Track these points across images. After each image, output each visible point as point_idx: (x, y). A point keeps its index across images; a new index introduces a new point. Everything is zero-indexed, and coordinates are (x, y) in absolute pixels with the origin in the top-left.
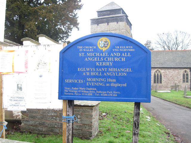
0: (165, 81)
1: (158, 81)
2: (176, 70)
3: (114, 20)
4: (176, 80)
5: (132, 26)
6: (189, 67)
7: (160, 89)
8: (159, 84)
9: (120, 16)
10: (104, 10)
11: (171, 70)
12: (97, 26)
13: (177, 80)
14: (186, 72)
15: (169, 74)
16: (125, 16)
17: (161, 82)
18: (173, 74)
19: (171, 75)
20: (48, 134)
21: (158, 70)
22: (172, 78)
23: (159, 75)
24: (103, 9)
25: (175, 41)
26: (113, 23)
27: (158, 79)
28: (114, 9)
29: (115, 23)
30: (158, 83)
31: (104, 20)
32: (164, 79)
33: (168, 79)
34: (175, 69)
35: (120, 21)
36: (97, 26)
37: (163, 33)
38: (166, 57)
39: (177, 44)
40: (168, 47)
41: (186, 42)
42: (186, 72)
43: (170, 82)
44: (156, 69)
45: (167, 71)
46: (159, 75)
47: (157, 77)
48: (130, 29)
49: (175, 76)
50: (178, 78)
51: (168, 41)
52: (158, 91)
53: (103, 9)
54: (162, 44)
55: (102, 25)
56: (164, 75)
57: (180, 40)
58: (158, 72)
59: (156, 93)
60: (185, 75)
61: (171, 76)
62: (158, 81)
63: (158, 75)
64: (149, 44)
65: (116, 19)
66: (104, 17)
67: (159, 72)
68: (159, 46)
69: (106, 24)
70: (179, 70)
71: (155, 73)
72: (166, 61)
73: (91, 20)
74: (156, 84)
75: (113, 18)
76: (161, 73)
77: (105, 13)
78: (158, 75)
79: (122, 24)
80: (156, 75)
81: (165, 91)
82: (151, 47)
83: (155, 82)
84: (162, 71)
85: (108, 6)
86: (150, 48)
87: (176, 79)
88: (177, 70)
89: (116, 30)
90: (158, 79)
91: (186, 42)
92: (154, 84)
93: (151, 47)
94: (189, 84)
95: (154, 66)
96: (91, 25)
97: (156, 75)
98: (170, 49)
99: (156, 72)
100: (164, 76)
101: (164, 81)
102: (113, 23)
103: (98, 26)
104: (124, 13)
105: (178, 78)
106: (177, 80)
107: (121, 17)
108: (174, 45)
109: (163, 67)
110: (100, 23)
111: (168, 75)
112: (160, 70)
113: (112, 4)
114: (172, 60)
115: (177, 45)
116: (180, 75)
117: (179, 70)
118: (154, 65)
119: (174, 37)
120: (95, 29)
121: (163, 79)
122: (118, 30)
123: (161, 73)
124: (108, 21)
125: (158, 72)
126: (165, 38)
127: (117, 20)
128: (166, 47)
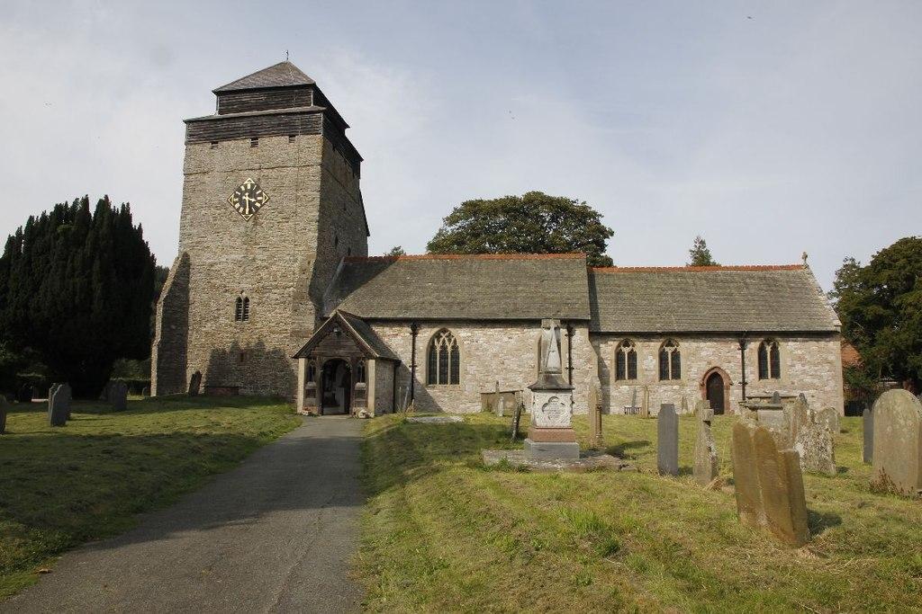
1: (443, 373)
5: (362, 164)
11: (494, 332)
26: (275, 139)
27: (444, 365)
30: (443, 381)
34: (529, 327)
45: (481, 335)
48: (350, 170)
58: (444, 336)
62: (443, 373)
63: (444, 348)
65: (285, 124)
69: (249, 141)
75: (275, 121)
76: (455, 341)
77: (245, 98)
78: (444, 348)
84: (461, 334)
90: (444, 365)
99: (437, 336)
113: (283, 67)
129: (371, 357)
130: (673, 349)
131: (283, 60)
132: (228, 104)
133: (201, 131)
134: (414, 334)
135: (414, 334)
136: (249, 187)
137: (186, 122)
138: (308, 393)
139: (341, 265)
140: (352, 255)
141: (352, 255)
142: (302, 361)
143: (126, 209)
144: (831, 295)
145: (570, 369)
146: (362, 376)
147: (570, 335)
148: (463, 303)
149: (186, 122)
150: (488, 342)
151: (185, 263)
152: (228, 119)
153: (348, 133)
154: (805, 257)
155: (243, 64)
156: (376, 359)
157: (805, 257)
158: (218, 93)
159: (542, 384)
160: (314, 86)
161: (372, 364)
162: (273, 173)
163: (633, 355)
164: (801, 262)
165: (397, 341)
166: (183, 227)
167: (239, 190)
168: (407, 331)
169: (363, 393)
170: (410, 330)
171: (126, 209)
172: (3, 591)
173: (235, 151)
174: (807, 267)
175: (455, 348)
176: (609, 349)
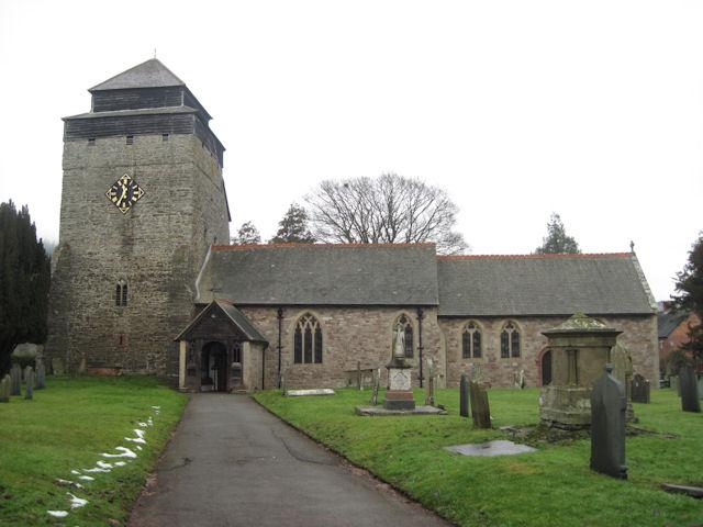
0: (335, 356)
1: (308, 354)
2: (371, 313)
3: (152, 125)
4: (373, 351)
5: (225, 153)
6: (413, 302)
7: (316, 382)
8: (314, 366)
9: (174, 114)
10: (116, 87)
11: (354, 316)
12: (89, 144)
13: (376, 349)
14: (403, 320)
15: (346, 328)
16: (196, 114)
17: (319, 360)
18: (360, 329)
19: (354, 333)
20: (677, 509)
21: (308, 315)
22: (357, 341)
23: (313, 332)
24: (116, 84)
25: (385, 214)
26: (149, 137)
27: (308, 345)
28: (154, 86)
29: (158, 138)
30: (308, 361)
31: (117, 123)
32: (330, 349)
33: (345, 348)
34: (369, 310)
35: (177, 132)
36: (89, 144)
37: (346, 186)
38: (340, 269)
39: (391, 222)
40: (364, 234)
41: (422, 217)
42: (403, 320)
43: (350, 358)
44: (302, 313)
45: (341, 319)
46: (313, 332)
47: (306, 339)
48: (215, 161)
49: (369, 337)
50: (377, 341)
51: (362, 213)
52: (291, 392)
53: (116, 84)
54: (340, 222)
55: (107, 141)
56: (329, 334)
57: (401, 211)
58: (308, 320)
59: (283, 399)
60: (510, 337)
61: (354, 337)
62: (308, 354)
63: (308, 331)
64: (298, 222)
65: (159, 124)
66: (116, 113)
67: (314, 320)
68: (330, 229)
69: (125, 139)
70: (381, 314)
71: (298, 326)
72: (339, 279)
73: (66, 120)
74: (303, 365)
75: (148, 121)
76: (318, 325)
78: (308, 331)
79: (182, 143)
80: (303, 332)
81: (314, 391)
82: (305, 233)
83: (298, 360)
84: (324, 318)
85: (137, 73)
86: (302, 237)
87: (371, 347)
88: (376, 312)
89: (159, 163)
90: (308, 345)
91: (422, 217)
92: (297, 365)
93: (305, 233)
94: (415, 365)
95: (295, 298)
96: (65, 139)
97: (303, 332)
98: (371, 241)
99: (303, 321)
100: (331, 338)
101: (328, 352)
102: (149, 138)
103: (93, 144)
104: (191, 100)
105: (377, 341)
106: (376, 349)
107: (179, 117)
108: (383, 230)
109: (326, 302)
110: (101, 136)
111: (345, 332)
112: (315, 313)
113: (153, 66)
114: (360, 278)
115: (393, 228)
116: (383, 333)
117: (383, 315)
118: (293, 295)
119: (382, 199)
120: (79, 158)
121: (326, 347)
122: (167, 163)
123: (318, 325)
124: (130, 129)
125: (308, 320)
126: (351, 201)
127: (163, 126)
128: (353, 234)
129: (247, 340)
130: (512, 330)
131: (151, 57)
132: (103, 103)
133: (77, 128)
134: (280, 317)
135: (280, 317)
136: (126, 182)
137: (63, 119)
138: (190, 372)
139: (209, 254)
140: (217, 243)
141: (217, 243)
142: (183, 346)
143: (25, 210)
144: (379, 317)
145: (421, 348)
146: (238, 356)
147: (420, 317)
148: (325, 289)
149: (63, 119)
150: (347, 325)
151: (65, 246)
152: (106, 118)
153: (212, 125)
154: (632, 245)
155: (111, 65)
156: (250, 341)
157: (632, 245)
158: (94, 92)
159: (393, 364)
160: (184, 87)
161: (246, 345)
162: (149, 170)
163: (477, 336)
164: (629, 251)
165: (265, 324)
166: (62, 218)
167: (116, 185)
168: (274, 312)
169: (239, 372)
170: (276, 314)
171: (25, 210)
172: (3, 510)
173: (113, 146)
174: (634, 254)
175: (319, 331)
176: (459, 328)
